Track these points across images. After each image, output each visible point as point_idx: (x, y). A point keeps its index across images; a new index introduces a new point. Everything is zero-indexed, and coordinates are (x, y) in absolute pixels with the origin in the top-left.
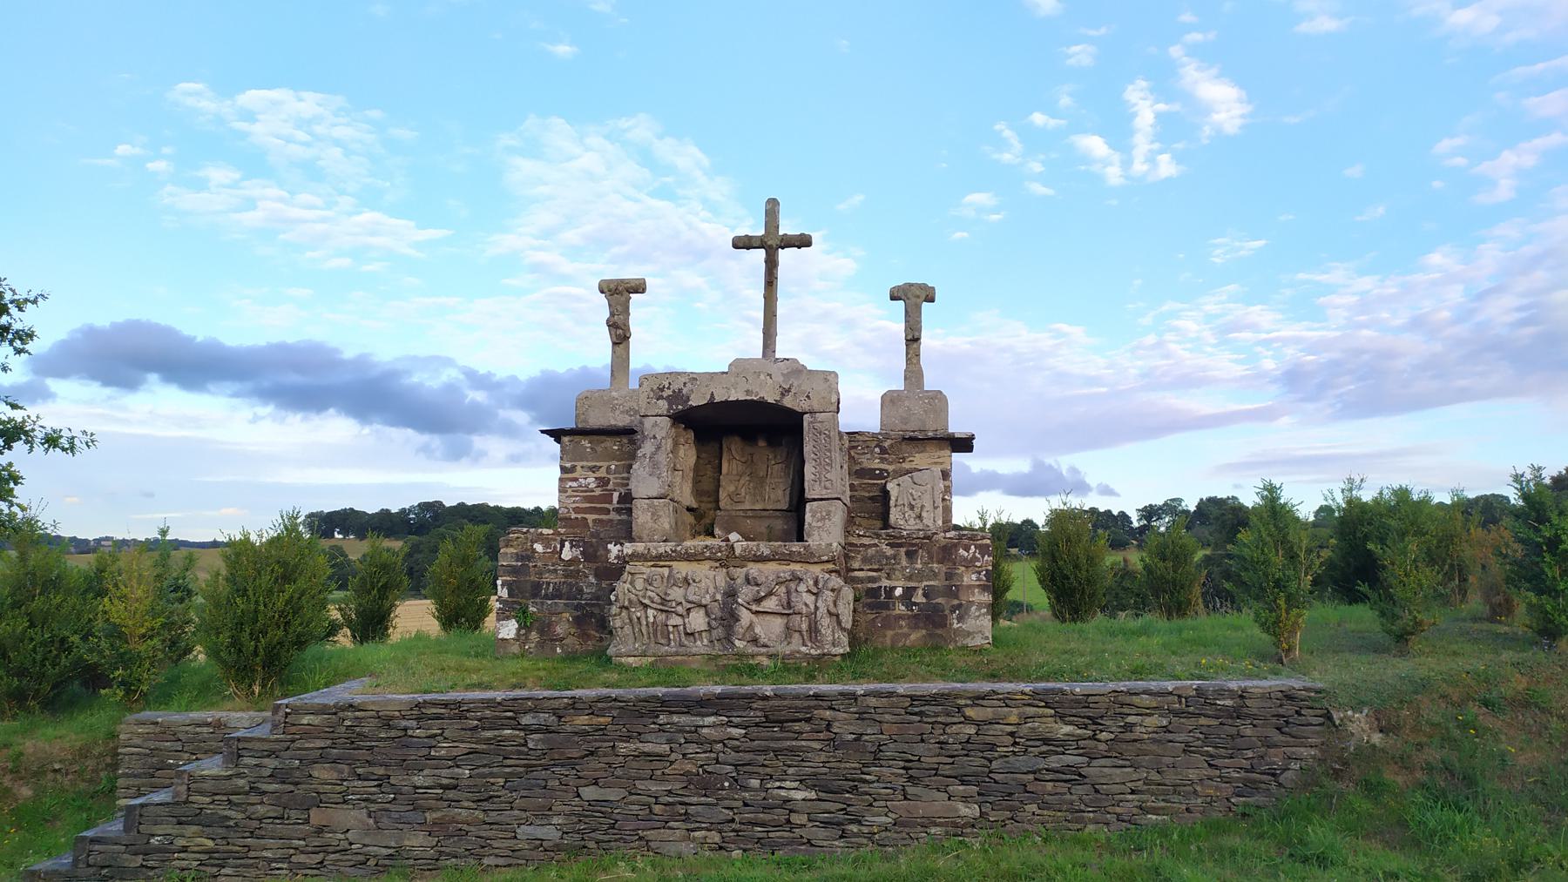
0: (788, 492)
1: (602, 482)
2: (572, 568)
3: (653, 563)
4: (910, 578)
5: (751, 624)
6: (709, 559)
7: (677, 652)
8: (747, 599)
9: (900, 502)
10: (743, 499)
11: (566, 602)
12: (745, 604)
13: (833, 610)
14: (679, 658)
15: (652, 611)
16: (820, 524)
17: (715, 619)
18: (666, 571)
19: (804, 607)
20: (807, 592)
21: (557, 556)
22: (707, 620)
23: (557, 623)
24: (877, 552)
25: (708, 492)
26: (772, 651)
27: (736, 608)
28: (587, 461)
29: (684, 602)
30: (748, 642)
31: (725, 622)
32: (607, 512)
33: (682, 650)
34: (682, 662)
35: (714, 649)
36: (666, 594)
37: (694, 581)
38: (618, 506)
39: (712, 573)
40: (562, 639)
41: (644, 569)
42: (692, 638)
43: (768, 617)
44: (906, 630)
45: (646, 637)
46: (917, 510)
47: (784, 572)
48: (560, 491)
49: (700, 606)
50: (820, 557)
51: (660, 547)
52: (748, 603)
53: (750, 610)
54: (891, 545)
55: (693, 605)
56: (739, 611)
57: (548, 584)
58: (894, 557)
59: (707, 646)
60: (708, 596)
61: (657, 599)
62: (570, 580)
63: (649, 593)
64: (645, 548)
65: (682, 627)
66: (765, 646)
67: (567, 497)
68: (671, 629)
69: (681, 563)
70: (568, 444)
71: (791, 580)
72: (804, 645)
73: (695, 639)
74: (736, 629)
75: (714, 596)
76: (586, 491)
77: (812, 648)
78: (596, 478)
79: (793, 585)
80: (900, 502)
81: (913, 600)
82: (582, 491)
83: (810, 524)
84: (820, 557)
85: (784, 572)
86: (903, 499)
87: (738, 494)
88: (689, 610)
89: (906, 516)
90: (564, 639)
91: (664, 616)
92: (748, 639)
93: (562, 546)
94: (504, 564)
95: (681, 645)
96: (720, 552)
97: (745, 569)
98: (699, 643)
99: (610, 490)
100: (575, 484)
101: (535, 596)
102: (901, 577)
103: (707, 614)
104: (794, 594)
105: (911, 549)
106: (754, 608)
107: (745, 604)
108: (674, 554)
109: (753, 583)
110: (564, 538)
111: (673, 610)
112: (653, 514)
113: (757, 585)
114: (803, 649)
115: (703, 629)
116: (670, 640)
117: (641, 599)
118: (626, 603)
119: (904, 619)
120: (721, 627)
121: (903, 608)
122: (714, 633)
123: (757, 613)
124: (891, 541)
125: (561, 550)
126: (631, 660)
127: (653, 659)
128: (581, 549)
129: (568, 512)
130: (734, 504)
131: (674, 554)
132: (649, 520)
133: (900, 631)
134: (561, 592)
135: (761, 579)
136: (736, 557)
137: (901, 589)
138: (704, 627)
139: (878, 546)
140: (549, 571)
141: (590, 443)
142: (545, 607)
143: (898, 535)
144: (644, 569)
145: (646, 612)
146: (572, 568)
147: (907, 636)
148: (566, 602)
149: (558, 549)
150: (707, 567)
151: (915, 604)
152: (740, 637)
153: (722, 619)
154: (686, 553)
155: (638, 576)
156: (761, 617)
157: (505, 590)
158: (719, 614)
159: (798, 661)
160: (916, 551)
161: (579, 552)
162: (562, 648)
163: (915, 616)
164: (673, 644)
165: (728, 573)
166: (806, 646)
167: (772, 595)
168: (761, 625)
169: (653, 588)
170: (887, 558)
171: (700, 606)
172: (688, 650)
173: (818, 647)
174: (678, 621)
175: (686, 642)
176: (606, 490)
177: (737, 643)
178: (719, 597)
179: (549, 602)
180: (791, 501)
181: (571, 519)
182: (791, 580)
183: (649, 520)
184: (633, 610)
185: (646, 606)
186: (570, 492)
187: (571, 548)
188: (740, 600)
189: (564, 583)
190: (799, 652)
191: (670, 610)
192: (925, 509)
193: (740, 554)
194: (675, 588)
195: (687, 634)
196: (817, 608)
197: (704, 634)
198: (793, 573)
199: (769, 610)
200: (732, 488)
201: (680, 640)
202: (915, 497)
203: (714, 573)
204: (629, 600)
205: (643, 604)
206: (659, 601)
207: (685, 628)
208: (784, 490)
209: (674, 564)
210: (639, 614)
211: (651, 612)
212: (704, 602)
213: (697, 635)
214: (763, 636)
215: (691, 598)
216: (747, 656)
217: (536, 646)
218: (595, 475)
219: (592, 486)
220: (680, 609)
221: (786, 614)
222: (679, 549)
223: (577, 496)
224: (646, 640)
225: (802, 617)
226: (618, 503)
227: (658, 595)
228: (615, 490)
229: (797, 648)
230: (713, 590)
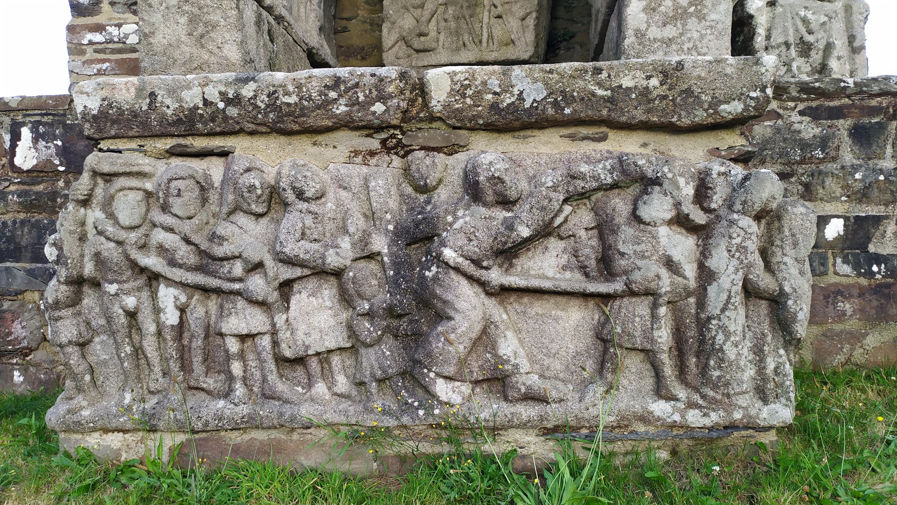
0: (531, 22)
2: (40, 188)
3: (168, 143)
4: (863, 195)
5: (484, 331)
6: (346, 124)
7: (251, 418)
8: (472, 248)
9: (778, 38)
10: (434, 45)
11: (28, 266)
12: (466, 265)
13: (765, 282)
14: (260, 435)
15: (173, 291)
16: (670, 32)
17: (369, 315)
18: (215, 169)
19: (664, 273)
20: (670, 223)
21: (4, 160)
22: (345, 316)
23: (15, 316)
24: (778, 131)
25: (363, 49)
26: (555, 413)
27: (435, 279)
29: (269, 262)
30: (477, 383)
31: (404, 324)
33: (270, 410)
34: (264, 450)
35: (369, 411)
36: (214, 237)
37: (300, 195)
39: (357, 171)
40: (25, 353)
41: (144, 163)
42: (300, 372)
43: (538, 307)
44: (853, 324)
45: (157, 369)
46: (816, 57)
47: (588, 160)
48: (71, 52)
49: (321, 272)
50: (715, 104)
51: (188, 87)
52: (477, 263)
53: (482, 284)
54: (814, 114)
55: (298, 272)
56: (448, 288)
58: (824, 142)
59: (347, 397)
60: (345, 244)
61: (184, 252)
62: (37, 217)
63: (160, 236)
64: (140, 90)
65: (265, 342)
66: (539, 399)
67: (84, 63)
68: (233, 346)
69: (259, 143)
71: (615, 186)
72: (661, 391)
73: (310, 377)
74: (438, 345)
75: (364, 240)
76: (120, 51)
77: (691, 405)
79: (620, 204)
80: (778, 38)
81: (872, 248)
82: (113, 51)
83: (640, 35)
84: (715, 104)
85: (588, 160)
86: (785, 31)
87: (421, 35)
88: (286, 288)
89: (794, 68)
90: (31, 350)
91: (213, 304)
92: (477, 375)
93: (16, 137)
95: (268, 396)
96: (383, 98)
97: (461, 158)
98: (320, 388)
100: (98, 37)
102: (839, 191)
103: (346, 299)
104: (628, 232)
105: (866, 120)
106: (496, 276)
107: (466, 265)
108: (233, 111)
109: (490, 197)
110: (20, 118)
111: (237, 286)
112: (193, 20)
113: (505, 202)
114: (660, 408)
115: (332, 345)
116: (231, 378)
117: (135, 255)
118: (89, 269)
119: (847, 297)
120: (389, 341)
121: (846, 269)
122: (370, 358)
123: (504, 292)
124: (814, 104)
125: (14, 146)
126: (114, 440)
127: (181, 438)
128: (60, 143)
130: (415, 55)
131: (233, 111)
132: (184, 38)
133: (838, 327)
135: (518, 185)
136: (432, 118)
137: (841, 222)
138: (336, 339)
139: (779, 116)
143: (831, 88)
144: (144, 163)
145: (154, 296)
146: (40, 188)
147: (856, 338)
148: (28, 266)
149: (7, 145)
150: (343, 151)
151: (878, 259)
152: (451, 370)
153: (391, 312)
154: (272, 106)
155: (122, 182)
156: (516, 305)
157: (432, 268)
158: (383, 298)
159: (641, 447)
160: (881, 127)
161: (53, 151)
162: (24, 371)
163: (879, 290)
164: (240, 390)
165: (406, 170)
166: (671, 398)
167: (548, 235)
168: (518, 331)
169: (168, 220)
170: (804, 145)
171: (321, 272)
172: (288, 410)
173: (714, 404)
174: (254, 321)
175: (281, 387)
177: (442, 389)
178: (380, 244)
180: (537, 46)
182: (615, 186)
183: (184, 38)
184: (112, 288)
185: (153, 278)
186: (90, 54)
187: (35, 140)
188: (449, 254)
189: (23, 223)
190: (645, 418)
191: (227, 286)
192: (835, 53)
193: (446, 106)
194: (242, 219)
195: (281, 361)
196: (706, 275)
197: (336, 360)
198: (621, 162)
199: (547, 285)
200: (407, 22)
201: (264, 380)
202: (813, 26)
203: (365, 169)
204: (98, 257)
205: (143, 270)
206: (193, 260)
207: (275, 343)
208: (523, 19)
209: (239, 144)
210: (130, 302)
211: (168, 296)
212: (333, 260)
213: (314, 364)
214: (525, 365)
215: (292, 248)
216: (475, 430)
220: (257, 284)
221: (592, 295)
222: (247, 91)
223: (104, 61)
224: (155, 379)
225: (655, 306)
227: (188, 241)
229: (638, 408)
230: (361, 223)
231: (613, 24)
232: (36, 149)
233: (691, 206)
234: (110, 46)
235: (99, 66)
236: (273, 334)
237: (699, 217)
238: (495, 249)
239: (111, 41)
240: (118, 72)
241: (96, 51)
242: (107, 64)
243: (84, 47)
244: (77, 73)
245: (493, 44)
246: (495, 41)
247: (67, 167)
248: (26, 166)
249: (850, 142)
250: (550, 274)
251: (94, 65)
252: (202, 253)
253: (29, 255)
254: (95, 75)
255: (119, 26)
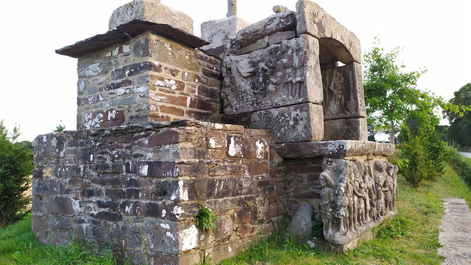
1: (181, 86)
28: (170, 64)
32: (182, 113)
38: (189, 109)
57: (220, 181)
67: (156, 94)
70: (155, 42)
78: (176, 81)
82: (167, 92)
93: (229, 142)
94: (185, 161)
99: (185, 94)
100: (161, 83)
101: (210, 195)
125: (228, 146)
129: (157, 110)
134: (228, 189)
140: (221, 168)
141: (171, 47)
142: (217, 206)
176: (183, 94)
179: (220, 200)
181: (158, 116)
217: (214, 251)
218: (175, 78)
219: (174, 88)
223: (163, 95)
226: (190, 106)
228: (188, 95)
232: (235, 147)
234: (165, 88)
235: (161, 97)
239: (165, 86)
240: (168, 102)
241: (160, 90)
242: (164, 97)
243: (156, 87)
244: (153, 99)
247: (244, 156)
248: (233, 155)
251: (159, 97)
253: (231, 193)
254: (159, 101)
255: (169, 80)
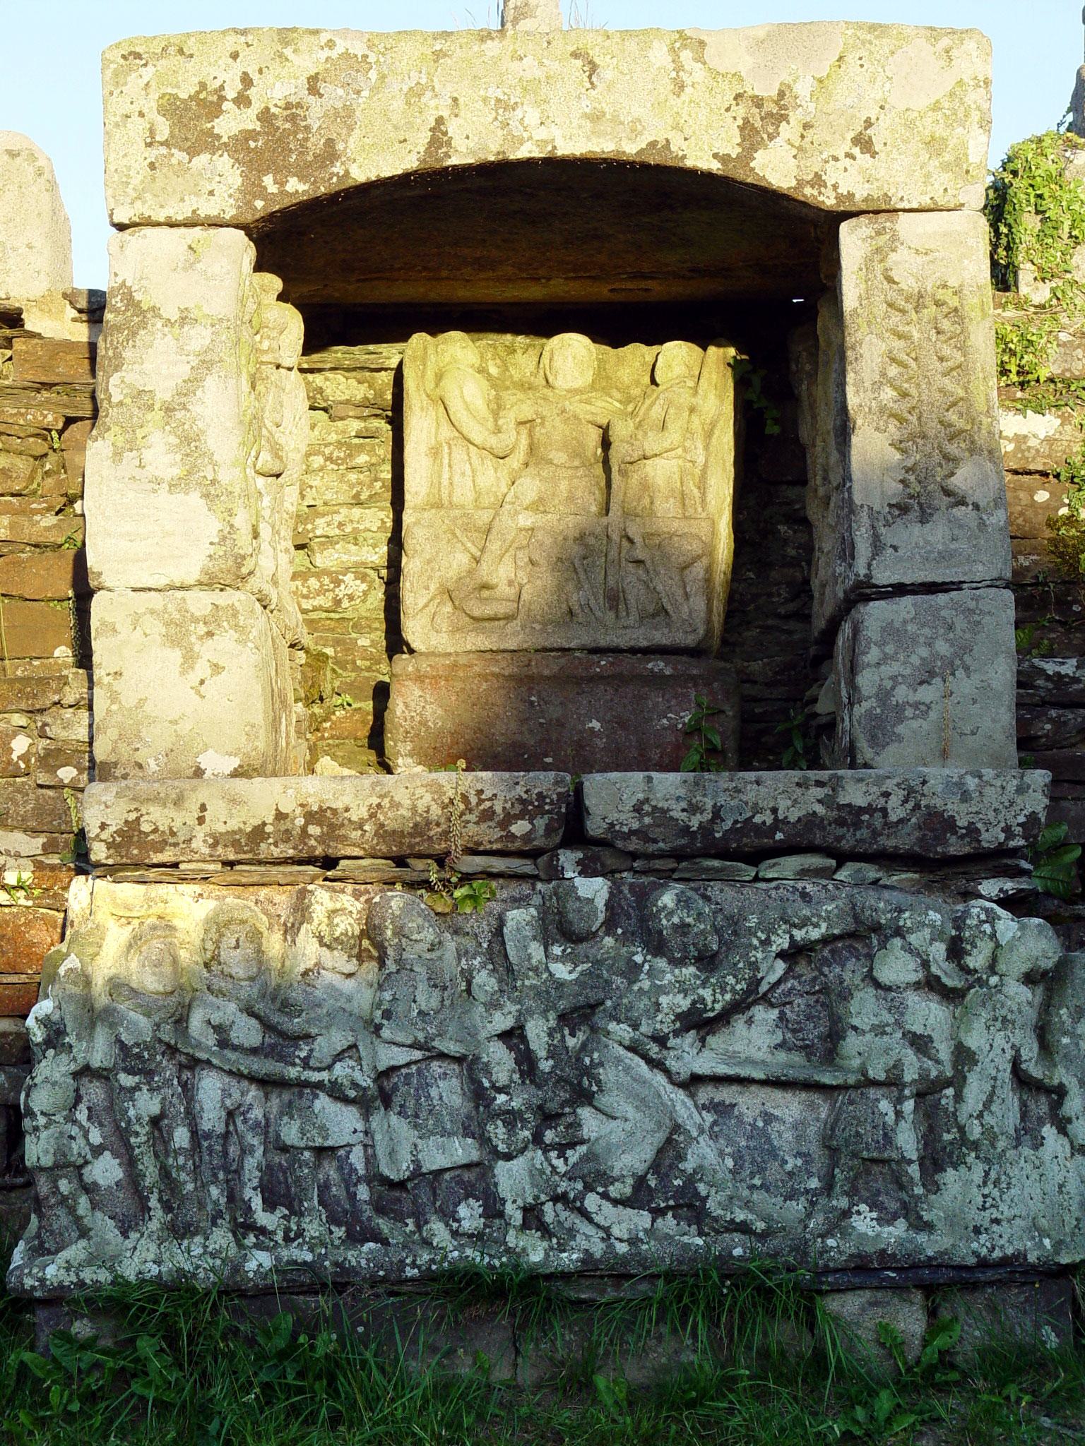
231: (847, 628)
233: (946, 965)
236: (365, 1146)
237: (952, 980)
238: (1058, 447)
245: (628, 614)
246: (633, 611)
249: (1010, 915)
250: (760, 1056)
252: (267, 1026)
